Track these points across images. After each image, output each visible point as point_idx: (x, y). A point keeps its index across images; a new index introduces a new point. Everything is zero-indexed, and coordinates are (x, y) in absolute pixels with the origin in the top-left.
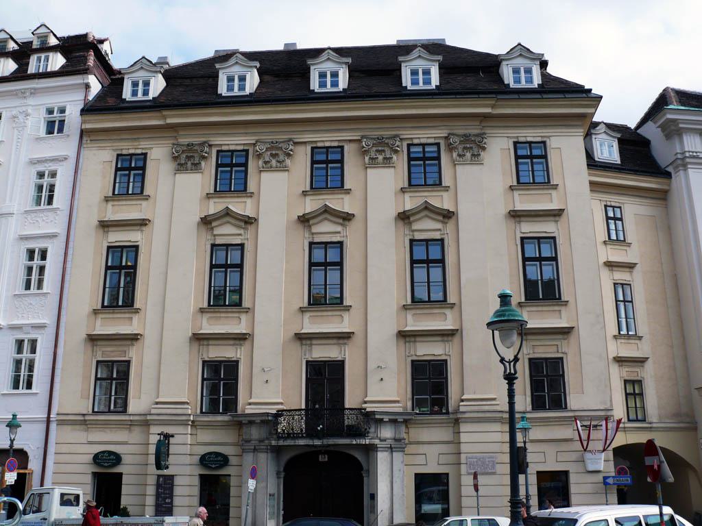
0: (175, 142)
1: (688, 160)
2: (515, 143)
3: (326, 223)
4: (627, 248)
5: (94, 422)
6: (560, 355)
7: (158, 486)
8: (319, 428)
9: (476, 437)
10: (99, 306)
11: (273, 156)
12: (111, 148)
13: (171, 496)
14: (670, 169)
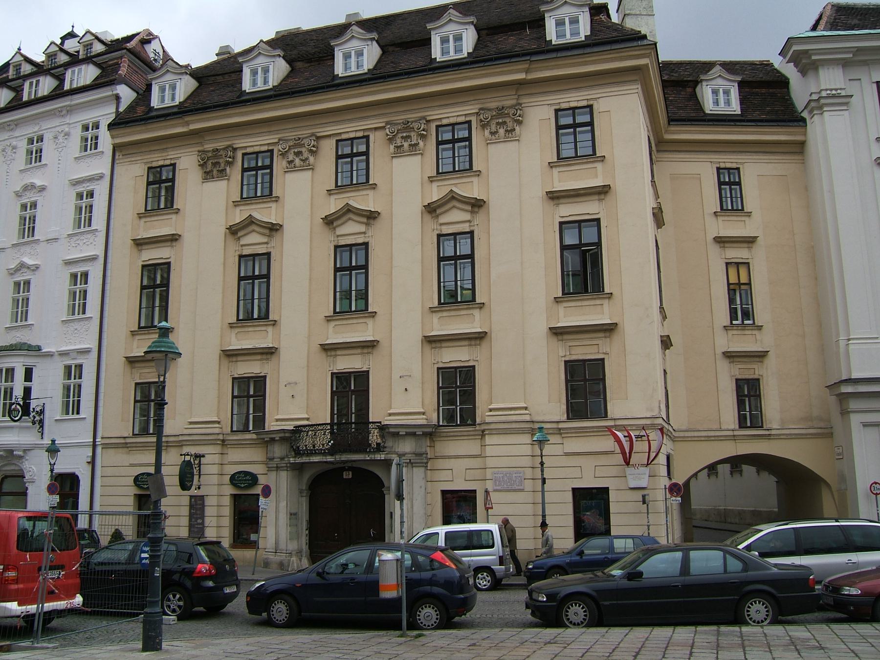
0: (200, 148)
1: (823, 101)
2: (557, 111)
3: (254, 234)
4: (746, 219)
6: (600, 356)
7: (191, 506)
9: (514, 450)
10: (136, 328)
13: (203, 517)
14: (805, 114)
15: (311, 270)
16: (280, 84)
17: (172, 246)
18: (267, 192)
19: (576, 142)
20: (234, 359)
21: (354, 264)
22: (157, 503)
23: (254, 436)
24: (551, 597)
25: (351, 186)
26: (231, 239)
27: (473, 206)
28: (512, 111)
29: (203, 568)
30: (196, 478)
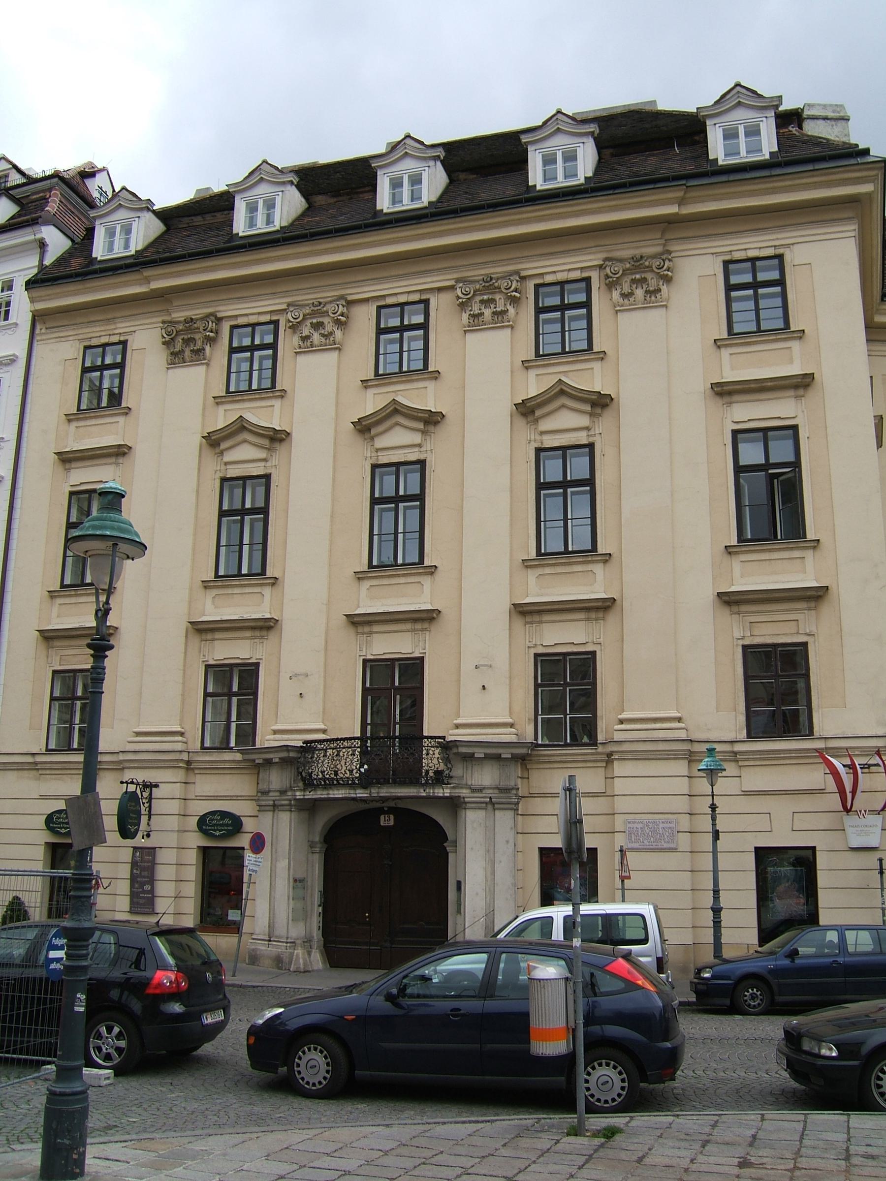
2: (726, 263)
3: (398, 429)
5: (48, 766)
7: (134, 864)
8: (366, 767)
10: (57, 587)
11: (317, 326)
12: (76, 337)
13: (152, 881)
15: (334, 500)
16: (292, 224)
17: (117, 464)
18: (267, 384)
19: (757, 310)
20: (209, 636)
21: (401, 493)
22: (84, 855)
23: (238, 757)
24: (846, 1049)
25: (402, 374)
26: (208, 453)
27: (594, 404)
28: (656, 263)
29: (166, 978)
30: (144, 819)
